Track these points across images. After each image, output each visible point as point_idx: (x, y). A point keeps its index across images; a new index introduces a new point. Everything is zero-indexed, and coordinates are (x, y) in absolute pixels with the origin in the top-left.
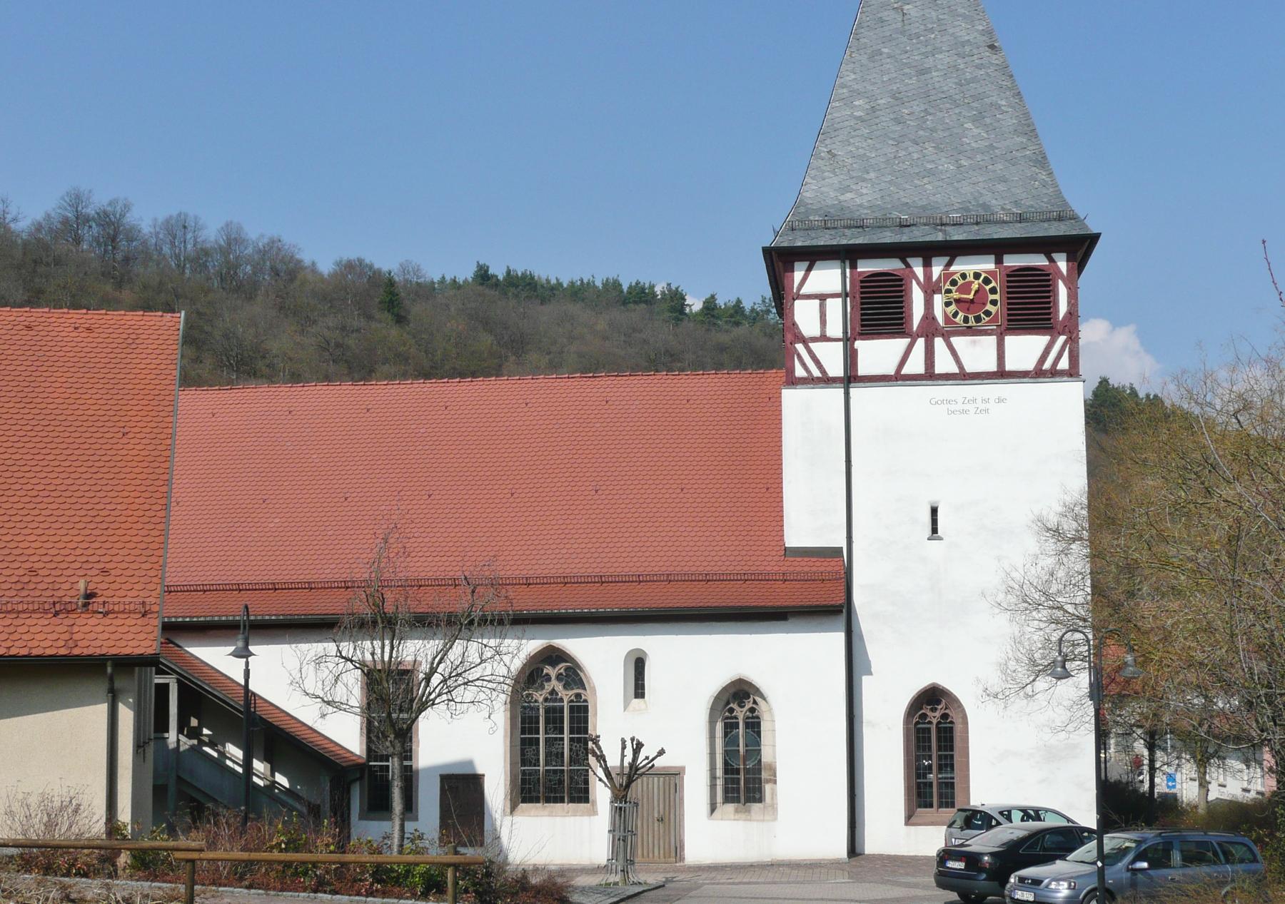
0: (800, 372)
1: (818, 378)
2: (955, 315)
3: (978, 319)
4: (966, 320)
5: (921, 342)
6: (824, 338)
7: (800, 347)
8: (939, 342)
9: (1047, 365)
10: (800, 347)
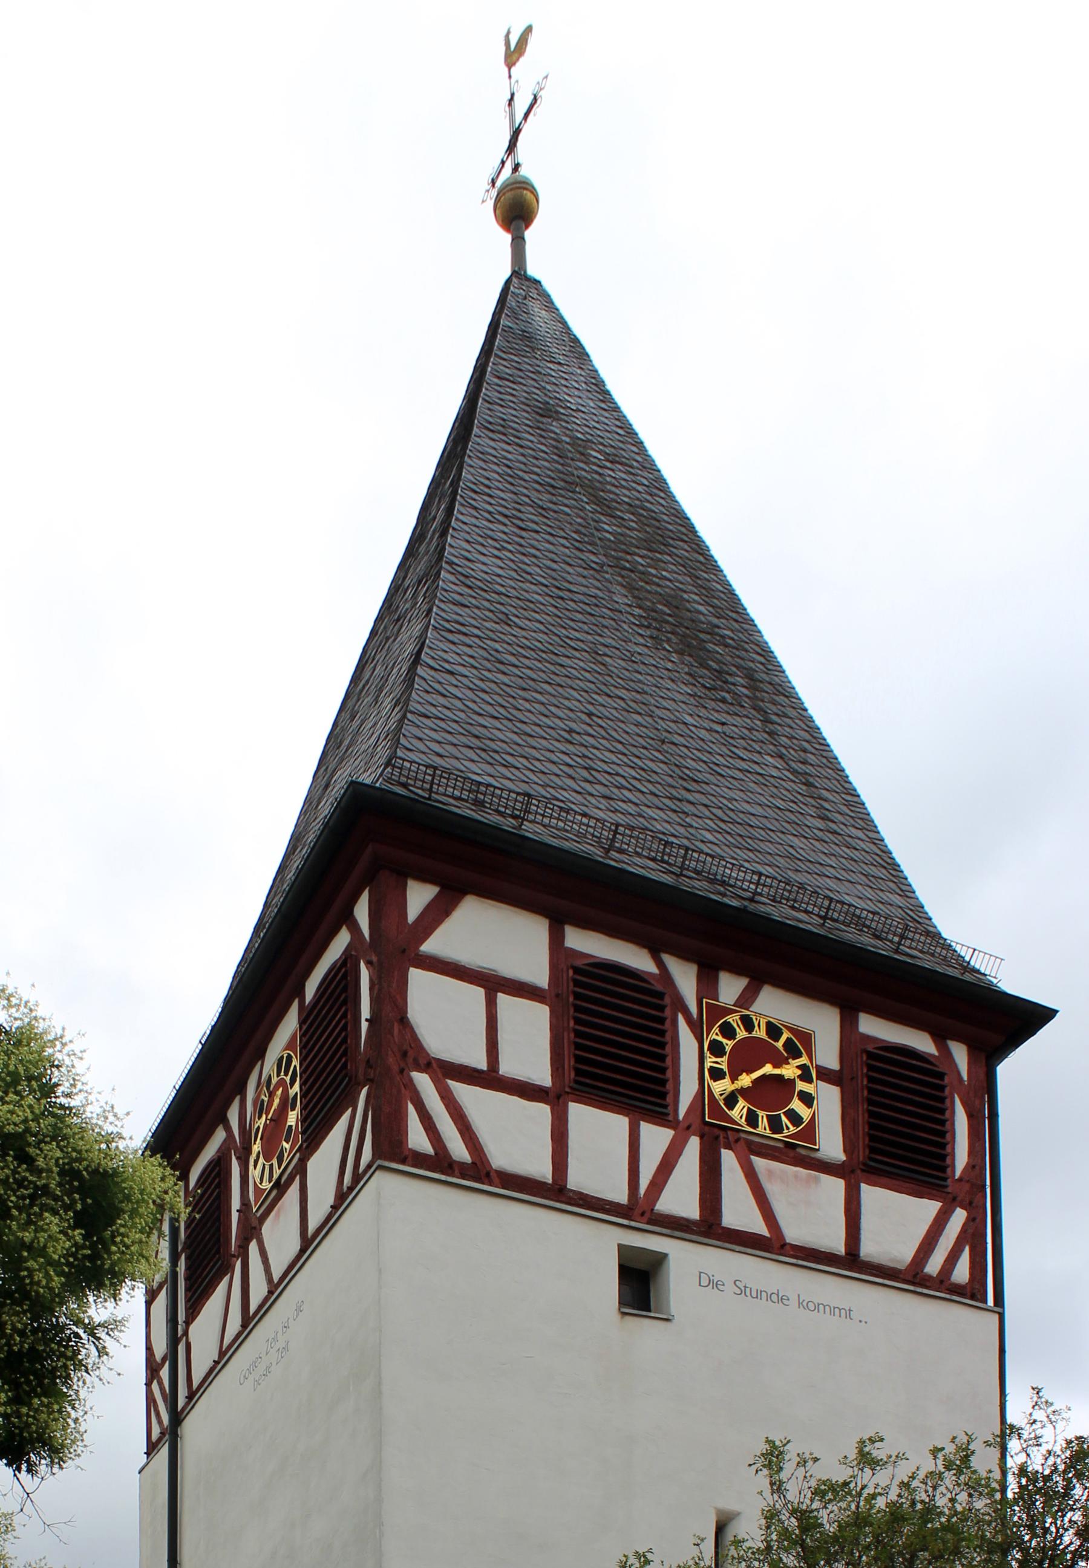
0: (417, 1139)
1: (462, 1165)
3: (775, 1125)
4: (752, 1120)
5: (693, 1146)
7: (423, 1081)
8: (728, 1159)
9: (934, 1266)
10: (423, 1081)
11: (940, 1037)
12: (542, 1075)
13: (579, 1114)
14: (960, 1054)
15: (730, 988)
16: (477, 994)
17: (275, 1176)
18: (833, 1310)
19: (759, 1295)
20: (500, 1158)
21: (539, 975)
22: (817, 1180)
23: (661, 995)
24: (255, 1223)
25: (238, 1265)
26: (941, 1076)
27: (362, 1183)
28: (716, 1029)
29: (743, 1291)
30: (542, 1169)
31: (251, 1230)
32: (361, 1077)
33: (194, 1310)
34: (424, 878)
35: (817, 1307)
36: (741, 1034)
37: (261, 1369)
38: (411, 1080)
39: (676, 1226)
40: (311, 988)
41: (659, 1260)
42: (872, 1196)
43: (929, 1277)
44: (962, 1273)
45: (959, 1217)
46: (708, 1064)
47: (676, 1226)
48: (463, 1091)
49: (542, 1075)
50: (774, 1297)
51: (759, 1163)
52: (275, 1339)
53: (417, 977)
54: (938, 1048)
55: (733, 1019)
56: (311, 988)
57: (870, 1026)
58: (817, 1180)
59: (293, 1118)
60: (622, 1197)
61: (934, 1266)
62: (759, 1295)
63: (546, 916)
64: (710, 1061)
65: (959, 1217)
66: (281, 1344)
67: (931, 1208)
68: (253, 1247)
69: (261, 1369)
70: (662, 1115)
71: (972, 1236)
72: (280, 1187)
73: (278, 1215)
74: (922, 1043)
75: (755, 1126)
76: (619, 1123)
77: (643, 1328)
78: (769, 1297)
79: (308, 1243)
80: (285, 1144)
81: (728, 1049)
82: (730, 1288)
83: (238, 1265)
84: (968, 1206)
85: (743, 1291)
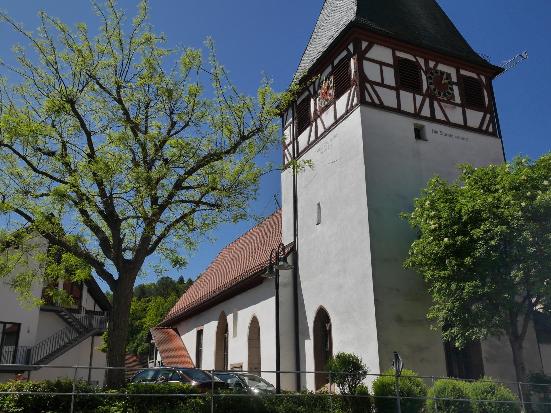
0: (368, 99)
1: (378, 104)
2: (435, 90)
6: (382, 85)
7: (368, 86)
8: (435, 103)
9: (484, 128)
10: (368, 86)
11: (478, 75)
12: (393, 84)
13: (402, 93)
14: (483, 78)
15: (432, 64)
16: (378, 66)
17: (326, 104)
18: (463, 138)
19: (446, 135)
20: (386, 103)
21: (391, 62)
22: (456, 108)
23: (417, 66)
24: (319, 114)
25: (314, 124)
26: (480, 84)
27: (354, 109)
28: (430, 73)
29: (442, 134)
30: (395, 106)
31: (317, 116)
32: (352, 83)
33: (300, 133)
34: (365, 41)
35: (459, 138)
36: (435, 74)
37: (323, 150)
38: (365, 85)
39: (425, 118)
40: (336, 62)
41: (422, 127)
42: (469, 112)
43: (483, 130)
44: (491, 129)
45: (488, 116)
46: (429, 81)
47: (425, 118)
48: (377, 88)
49: (393, 84)
50: (450, 136)
51: (442, 104)
52: (328, 143)
53: (365, 63)
54: (478, 77)
55: (433, 71)
56: (336, 62)
57: (463, 72)
58: (456, 108)
59: (331, 91)
60: (412, 111)
61: (484, 128)
62: (446, 135)
63: (391, 49)
64: (429, 81)
65: (488, 116)
66: (330, 144)
67: (481, 114)
68: (319, 120)
69: (323, 150)
70: (421, 93)
71: (491, 121)
72: (327, 107)
73: (327, 113)
74: (474, 76)
75: (441, 95)
76: (411, 95)
77: (422, 143)
78: (448, 135)
79: (337, 121)
80: (329, 97)
81: (433, 78)
82: (439, 133)
83: (314, 124)
84: (490, 114)
85: (442, 134)
